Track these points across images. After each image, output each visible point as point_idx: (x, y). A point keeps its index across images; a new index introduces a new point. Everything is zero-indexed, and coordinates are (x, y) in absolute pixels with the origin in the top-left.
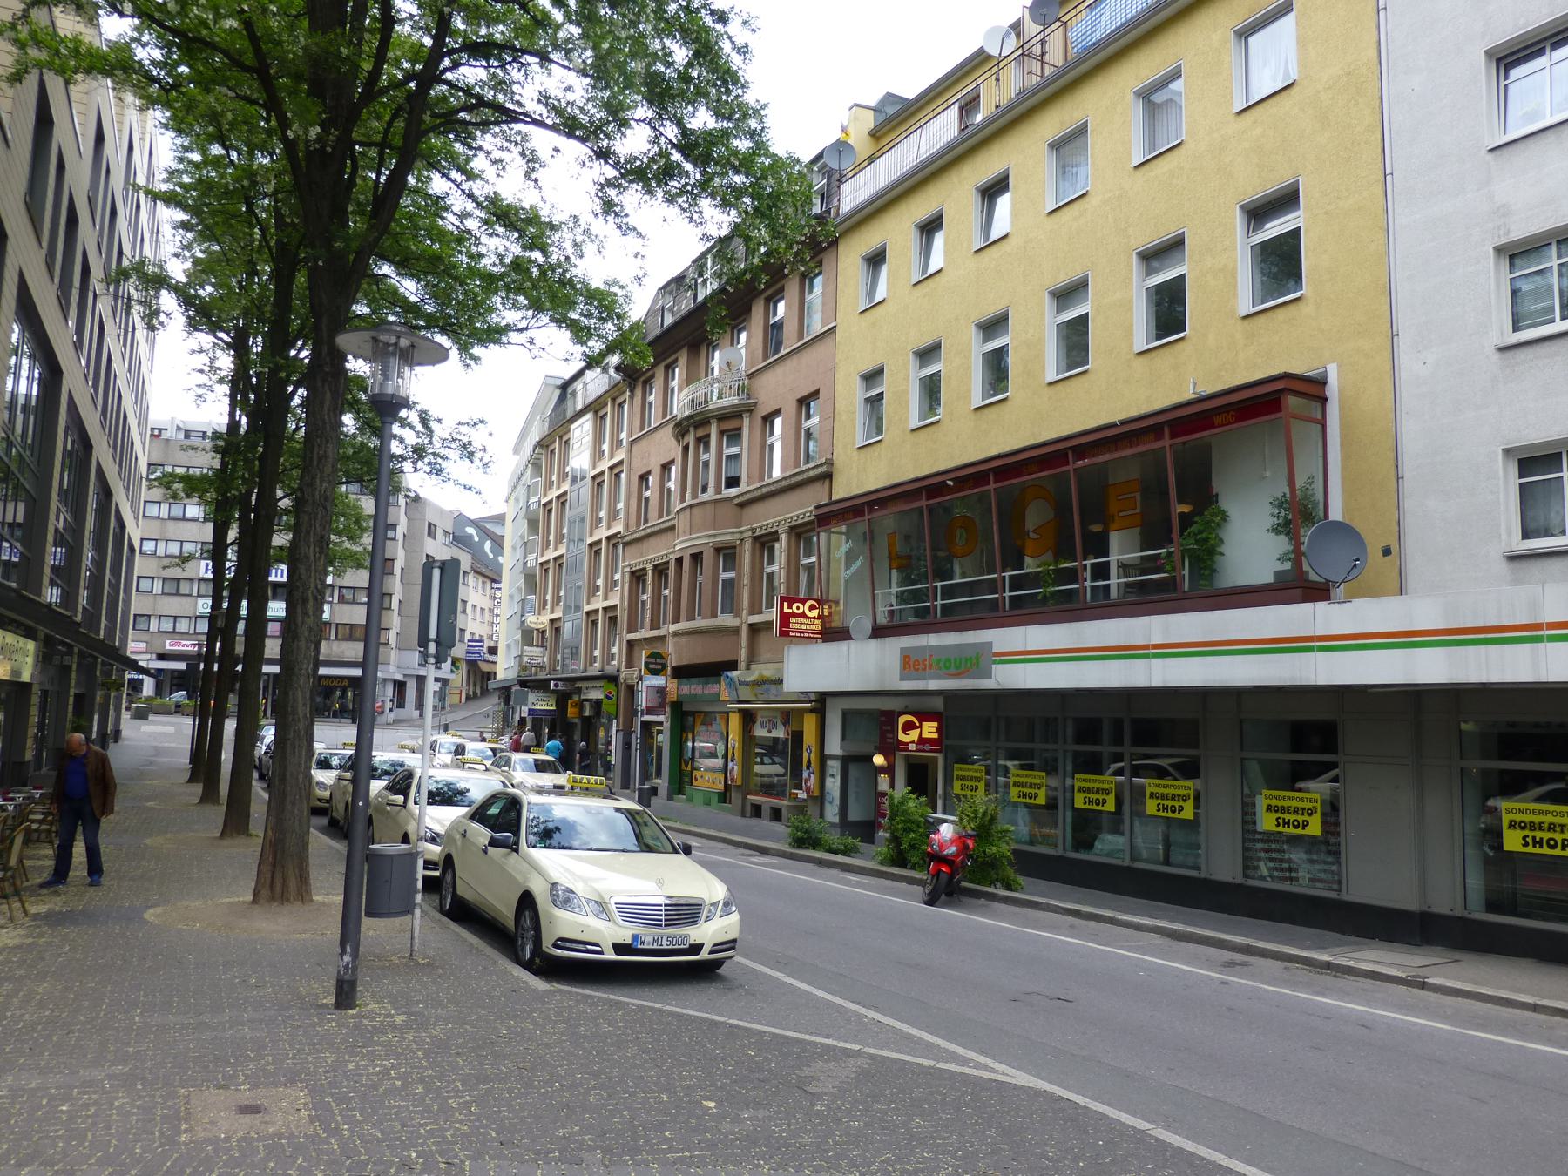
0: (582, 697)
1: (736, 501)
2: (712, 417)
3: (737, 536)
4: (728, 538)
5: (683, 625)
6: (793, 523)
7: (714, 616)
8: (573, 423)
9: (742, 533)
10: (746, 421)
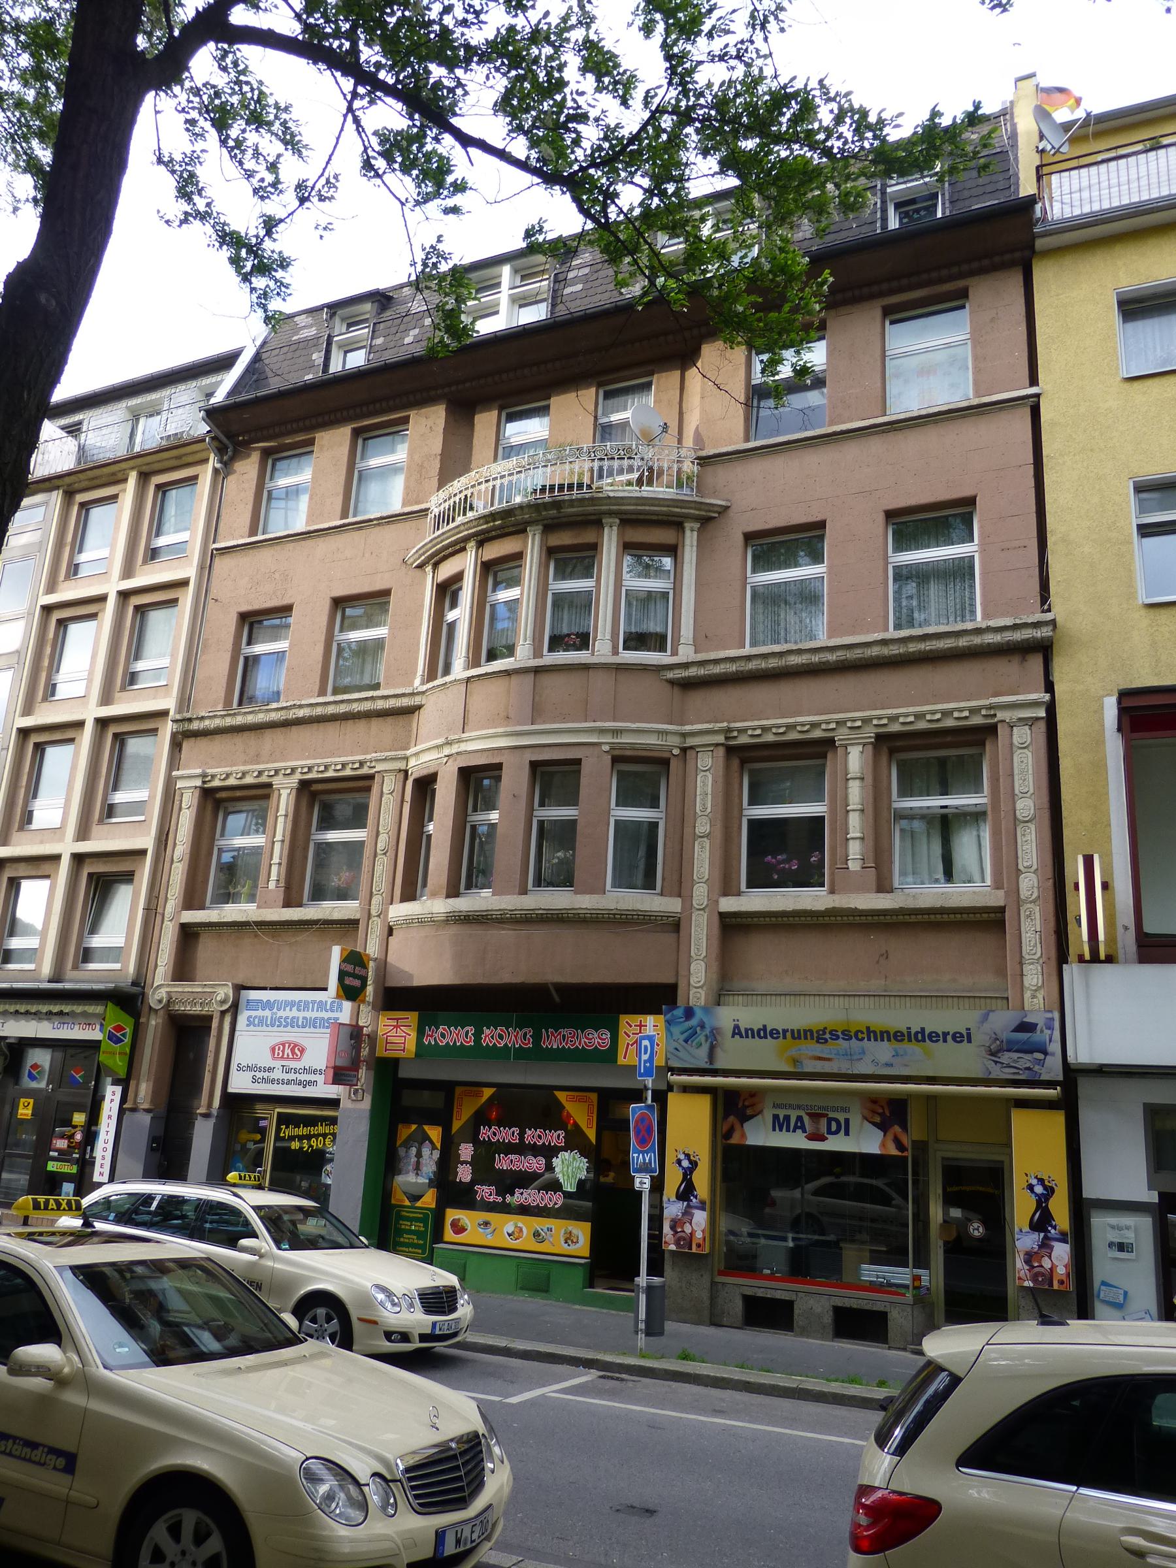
1: (670, 675)
2: (611, 514)
4: (652, 740)
6: (313, 775)
7: (524, 891)
9: (684, 735)
10: (690, 539)
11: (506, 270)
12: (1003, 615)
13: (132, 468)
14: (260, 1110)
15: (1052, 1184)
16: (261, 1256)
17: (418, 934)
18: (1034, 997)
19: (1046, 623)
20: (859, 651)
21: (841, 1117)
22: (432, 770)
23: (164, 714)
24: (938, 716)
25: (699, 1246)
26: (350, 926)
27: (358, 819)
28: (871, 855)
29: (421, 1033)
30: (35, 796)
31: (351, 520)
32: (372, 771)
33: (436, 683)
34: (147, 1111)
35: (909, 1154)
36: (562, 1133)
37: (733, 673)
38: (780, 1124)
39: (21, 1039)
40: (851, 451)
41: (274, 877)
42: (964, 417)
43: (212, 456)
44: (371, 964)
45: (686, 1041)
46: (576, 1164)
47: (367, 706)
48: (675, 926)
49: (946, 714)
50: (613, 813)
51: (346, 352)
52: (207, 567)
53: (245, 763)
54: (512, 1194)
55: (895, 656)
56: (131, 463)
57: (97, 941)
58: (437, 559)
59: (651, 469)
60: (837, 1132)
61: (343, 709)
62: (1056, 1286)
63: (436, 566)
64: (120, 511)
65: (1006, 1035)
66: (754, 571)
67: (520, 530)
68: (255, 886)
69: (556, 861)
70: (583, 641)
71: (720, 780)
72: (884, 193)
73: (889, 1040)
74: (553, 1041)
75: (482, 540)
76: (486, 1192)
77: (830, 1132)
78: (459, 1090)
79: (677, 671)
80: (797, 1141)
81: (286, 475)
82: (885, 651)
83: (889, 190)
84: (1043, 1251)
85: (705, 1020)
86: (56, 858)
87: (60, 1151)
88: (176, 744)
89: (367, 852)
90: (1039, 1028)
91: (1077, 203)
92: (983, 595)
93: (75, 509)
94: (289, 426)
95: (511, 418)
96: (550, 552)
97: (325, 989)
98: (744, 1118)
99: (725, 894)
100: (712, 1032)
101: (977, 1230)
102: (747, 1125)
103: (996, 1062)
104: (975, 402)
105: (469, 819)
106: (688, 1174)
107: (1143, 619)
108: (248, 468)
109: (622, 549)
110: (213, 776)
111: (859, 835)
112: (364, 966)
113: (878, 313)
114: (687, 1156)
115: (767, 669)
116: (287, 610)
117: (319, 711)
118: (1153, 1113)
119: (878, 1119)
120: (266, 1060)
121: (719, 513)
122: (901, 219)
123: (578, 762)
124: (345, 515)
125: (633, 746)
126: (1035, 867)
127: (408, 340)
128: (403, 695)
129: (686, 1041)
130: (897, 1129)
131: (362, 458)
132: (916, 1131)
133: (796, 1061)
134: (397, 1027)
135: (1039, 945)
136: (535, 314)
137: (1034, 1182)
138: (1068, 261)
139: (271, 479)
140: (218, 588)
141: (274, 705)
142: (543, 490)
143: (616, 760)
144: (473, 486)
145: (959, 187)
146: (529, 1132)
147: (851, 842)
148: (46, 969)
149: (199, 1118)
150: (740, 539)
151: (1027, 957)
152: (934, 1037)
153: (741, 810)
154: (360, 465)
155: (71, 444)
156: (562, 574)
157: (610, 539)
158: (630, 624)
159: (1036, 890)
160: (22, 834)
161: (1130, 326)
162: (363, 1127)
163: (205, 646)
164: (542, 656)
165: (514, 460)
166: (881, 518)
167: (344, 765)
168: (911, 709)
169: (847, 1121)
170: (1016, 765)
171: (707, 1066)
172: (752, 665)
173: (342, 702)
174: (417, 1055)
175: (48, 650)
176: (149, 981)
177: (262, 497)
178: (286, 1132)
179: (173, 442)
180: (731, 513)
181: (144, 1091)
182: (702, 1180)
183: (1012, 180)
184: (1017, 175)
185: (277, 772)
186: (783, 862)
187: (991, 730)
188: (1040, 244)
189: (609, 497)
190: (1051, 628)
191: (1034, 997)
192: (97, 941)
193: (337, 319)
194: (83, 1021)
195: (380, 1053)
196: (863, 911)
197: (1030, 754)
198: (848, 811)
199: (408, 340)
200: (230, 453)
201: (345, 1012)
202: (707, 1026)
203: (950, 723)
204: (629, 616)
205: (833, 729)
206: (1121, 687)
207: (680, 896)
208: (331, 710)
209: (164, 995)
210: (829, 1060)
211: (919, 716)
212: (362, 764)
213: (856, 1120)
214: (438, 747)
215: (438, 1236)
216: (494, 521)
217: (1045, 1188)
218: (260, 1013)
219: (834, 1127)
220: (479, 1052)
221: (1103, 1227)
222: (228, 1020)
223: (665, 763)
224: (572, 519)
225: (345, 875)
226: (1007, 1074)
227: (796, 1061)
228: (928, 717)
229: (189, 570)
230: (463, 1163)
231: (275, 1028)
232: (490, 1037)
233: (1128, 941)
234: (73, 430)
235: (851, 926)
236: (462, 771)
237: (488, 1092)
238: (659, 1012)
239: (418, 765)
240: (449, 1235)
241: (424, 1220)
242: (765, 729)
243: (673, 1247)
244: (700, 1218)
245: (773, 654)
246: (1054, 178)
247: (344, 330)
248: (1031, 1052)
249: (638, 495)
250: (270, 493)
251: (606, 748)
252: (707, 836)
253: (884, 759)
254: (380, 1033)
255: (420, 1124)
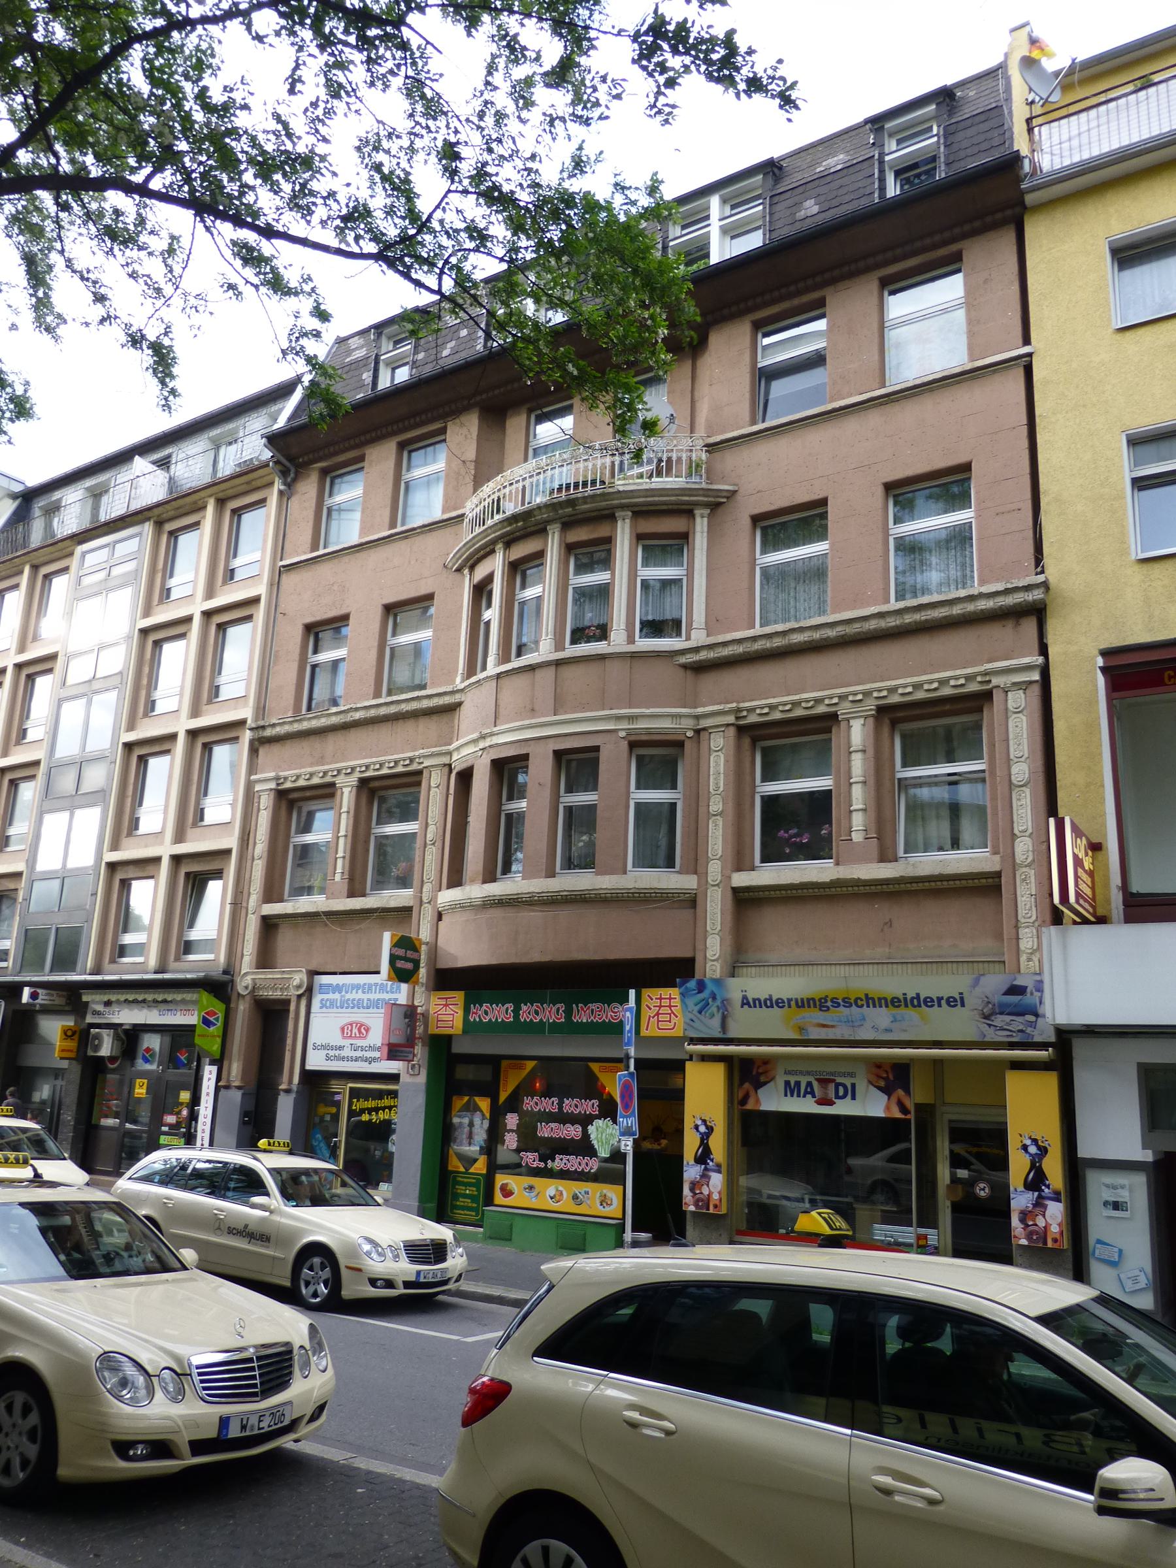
0: (89, 1019)
1: (683, 660)
2: (623, 507)
3: (689, 723)
4: (666, 724)
5: (475, 891)
7: (551, 874)
8: (81, 542)
9: (697, 717)
10: (701, 525)
11: (715, 201)
12: (998, 580)
13: (210, 496)
14: (335, 1086)
15: (1046, 1144)
16: (271, 1212)
17: (460, 918)
18: (1029, 960)
19: (1037, 586)
20: (857, 625)
21: (848, 1082)
22: (469, 764)
23: (242, 723)
24: (935, 685)
25: (716, 1206)
26: (404, 913)
27: (408, 812)
28: (873, 827)
29: (467, 1010)
30: (206, 794)
31: (399, 529)
32: (421, 767)
33: (473, 679)
34: (239, 1088)
35: (912, 1117)
36: (596, 1102)
37: (740, 655)
38: (792, 1090)
39: (135, 1025)
40: (851, 426)
41: (339, 870)
42: (958, 382)
43: (277, 479)
44: (424, 948)
45: (700, 1012)
46: (609, 1131)
47: (414, 706)
48: (691, 902)
49: (943, 682)
50: (632, 796)
51: (394, 369)
52: (275, 584)
53: (312, 765)
54: (553, 1160)
55: (892, 627)
56: (209, 491)
57: (194, 935)
58: (472, 562)
59: (669, 460)
60: (844, 1096)
61: (393, 709)
62: (1050, 1244)
63: (472, 568)
64: (202, 536)
65: (998, 998)
66: (764, 552)
67: (541, 531)
68: (325, 879)
69: (581, 844)
70: (603, 632)
71: (732, 759)
72: (881, 162)
73: (887, 1006)
74: (583, 1016)
75: (509, 542)
76: (531, 1159)
77: (838, 1097)
78: (504, 1063)
79: (688, 656)
80: (806, 1106)
81: (425, 464)
82: (883, 624)
83: (887, 158)
84: (1038, 1210)
85: (716, 991)
86: (157, 860)
87: (171, 1126)
88: (254, 751)
89: (419, 843)
90: (1028, 990)
91: (1066, 153)
92: (979, 561)
93: (164, 538)
94: (406, 423)
95: (540, 419)
96: (569, 548)
97: (378, 973)
98: (758, 1085)
99: (739, 869)
100: (722, 1002)
101: (982, 1191)
102: (760, 1091)
103: (990, 1025)
104: (969, 367)
105: (504, 808)
106: (705, 1139)
107: (1136, 575)
108: (308, 488)
109: (634, 541)
110: (286, 779)
111: (861, 806)
112: (416, 950)
113: (874, 285)
114: (704, 1121)
115: (772, 649)
116: (344, 618)
117: (372, 713)
118: (1148, 1074)
119: (882, 1084)
120: (337, 1040)
121: (728, 498)
122: (902, 186)
123: (596, 749)
124: (393, 525)
125: (648, 731)
126: (1030, 831)
127: (445, 353)
128: (445, 694)
129: (700, 1012)
130: (900, 1092)
131: (408, 470)
132: (920, 1094)
133: (801, 1029)
134: (446, 1005)
135: (1034, 909)
136: (754, 241)
137: (1028, 1142)
138: (1059, 214)
139: (331, 495)
140: (289, 603)
141: (334, 710)
142: (560, 489)
143: (633, 745)
144: (499, 490)
145: (955, 147)
146: (566, 1102)
147: (854, 814)
148: (153, 961)
149: (282, 1093)
150: (746, 522)
151: (1023, 920)
152: (929, 1002)
153: (754, 786)
154: (406, 476)
155: (161, 476)
156: (581, 568)
157: (623, 532)
158: (647, 614)
159: (1030, 854)
160: (131, 839)
161: (1128, 274)
162: (420, 1100)
163: (276, 656)
164: (564, 649)
165: (532, 463)
166: (880, 491)
167: (396, 762)
168: (909, 680)
169: (853, 1086)
170: (1010, 730)
171: (721, 1036)
172: (757, 646)
173: (392, 703)
174: (464, 1031)
175: (146, 670)
176: (237, 970)
177: (322, 515)
178: (358, 1105)
179: (244, 468)
180: (739, 497)
181: (235, 1069)
182: (718, 1143)
183: (1006, 134)
184: (1011, 129)
185: (339, 771)
186: (795, 836)
187: (987, 696)
188: (1029, 199)
189: (619, 492)
190: (1042, 590)
191: (1029, 960)
192: (194, 935)
193: (384, 339)
194: (183, 1007)
195: (433, 1030)
196: (865, 881)
197: (1024, 718)
198: (851, 784)
199: (445, 353)
200: (292, 475)
201: (401, 994)
202: (718, 997)
203: (947, 691)
204: (645, 602)
205: (836, 704)
206: (1102, 647)
207: (695, 873)
208: (383, 711)
209: (250, 982)
210: (833, 1026)
211: (917, 686)
212: (412, 760)
213: (862, 1086)
214: (475, 741)
215: (489, 1200)
216: (517, 522)
217: (1039, 1148)
218: (331, 996)
219: (841, 1092)
220: (518, 1028)
221: (1099, 1187)
222: (303, 1003)
223: (680, 744)
224: (588, 515)
225: (403, 865)
226: (1001, 1037)
227: (801, 1029)
228: (926, 687)
229: (260, 589)
230: (509, 1131)
231: (344, 1010)
232: (528, 1013)
233: (1117, 900)
234: (164, 464)
235: (856, 896)
236: (495, 763)
237: (530, 1065)
238: (674, 985)
239: (459, 761)
240: (499, 1198)
241: (476, 1185)
242: (772, 707)
243: (692, 1208)
244: (717, 1181)
245: (777, 634)
246: (1044, 129)
247: (391, 348)
248: (1022, 1014)
249: (647, 487)
250: (407, 483)
251: (622, 734)
252: (721, 814)
253: (886, 730)
254: (431, 1012)
255: (471, 1095)
